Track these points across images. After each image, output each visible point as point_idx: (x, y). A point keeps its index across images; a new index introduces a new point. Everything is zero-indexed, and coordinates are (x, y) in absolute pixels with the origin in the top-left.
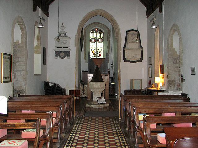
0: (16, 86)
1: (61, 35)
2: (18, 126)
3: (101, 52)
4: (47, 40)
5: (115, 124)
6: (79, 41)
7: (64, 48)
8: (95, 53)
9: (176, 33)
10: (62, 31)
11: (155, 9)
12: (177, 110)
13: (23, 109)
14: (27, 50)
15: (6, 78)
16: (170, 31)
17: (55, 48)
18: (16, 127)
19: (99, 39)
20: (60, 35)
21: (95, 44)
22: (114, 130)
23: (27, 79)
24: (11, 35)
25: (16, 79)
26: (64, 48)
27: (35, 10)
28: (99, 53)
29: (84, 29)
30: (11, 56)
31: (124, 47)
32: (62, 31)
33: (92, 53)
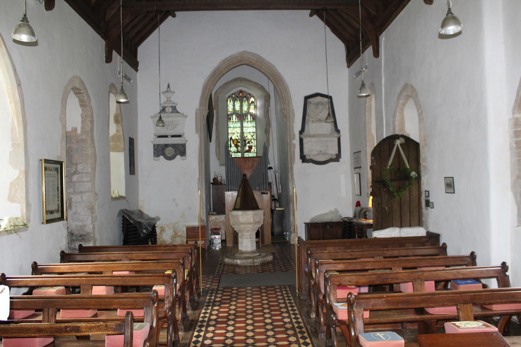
0: (74, 224)
1: (167, 109)
2: (87, 329)
3: (253, 141)
4: (136, 121)
5: (289, 305)
6: (205, 122)
7: (173, 136)
8: (239, 144)
9: (411, 103)
10: (168, 100)
11: (365, 49)
12: (417, 274)
13: (96, 283)
14: (95, 148)
15: (52, 212)
16: (398, 99)
17: (154, 137)
18: (81, 332)
19: (246, 115)
20: (163, 110)
21: (239, 125)
22: (287, 320)
23: (96, 209)
24: (61, 119)
25: (73, 210)
26: (173, 136)
27: (109, 59)
28: (248, 145)
29: (215, 94)
30: (61, 163)
31: (302, 132)
32: (168, 100)
33: (233, 145)
